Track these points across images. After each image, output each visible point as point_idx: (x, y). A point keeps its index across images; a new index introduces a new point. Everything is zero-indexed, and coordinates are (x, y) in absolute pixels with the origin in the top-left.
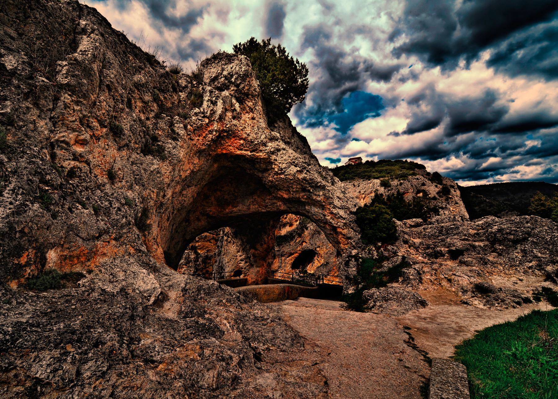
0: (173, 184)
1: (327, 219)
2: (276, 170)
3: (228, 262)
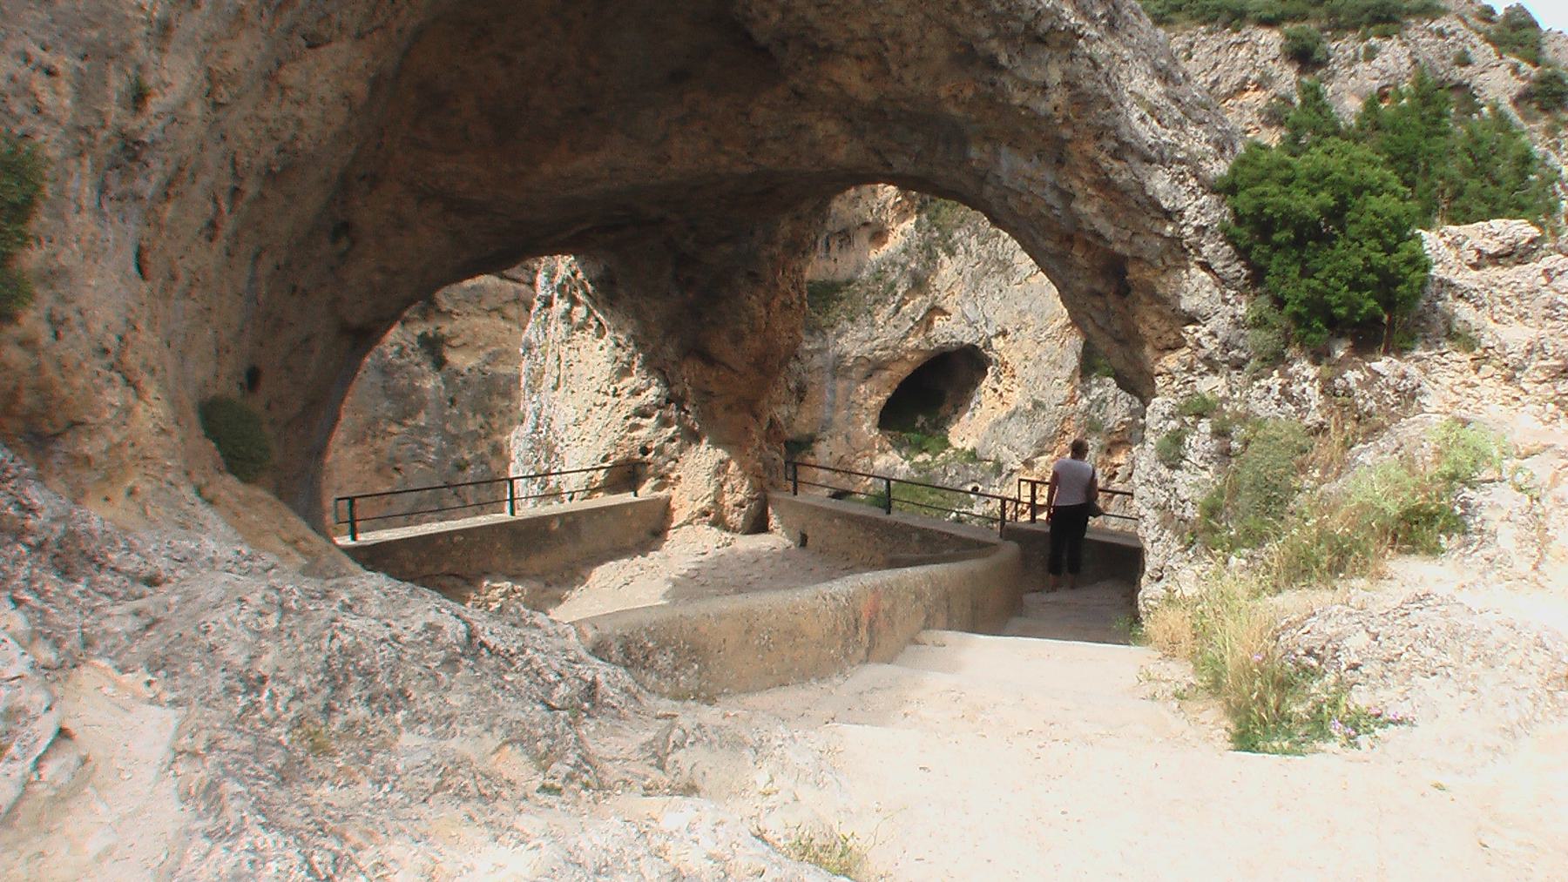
1: (1077, 219)
3: (577, 423)
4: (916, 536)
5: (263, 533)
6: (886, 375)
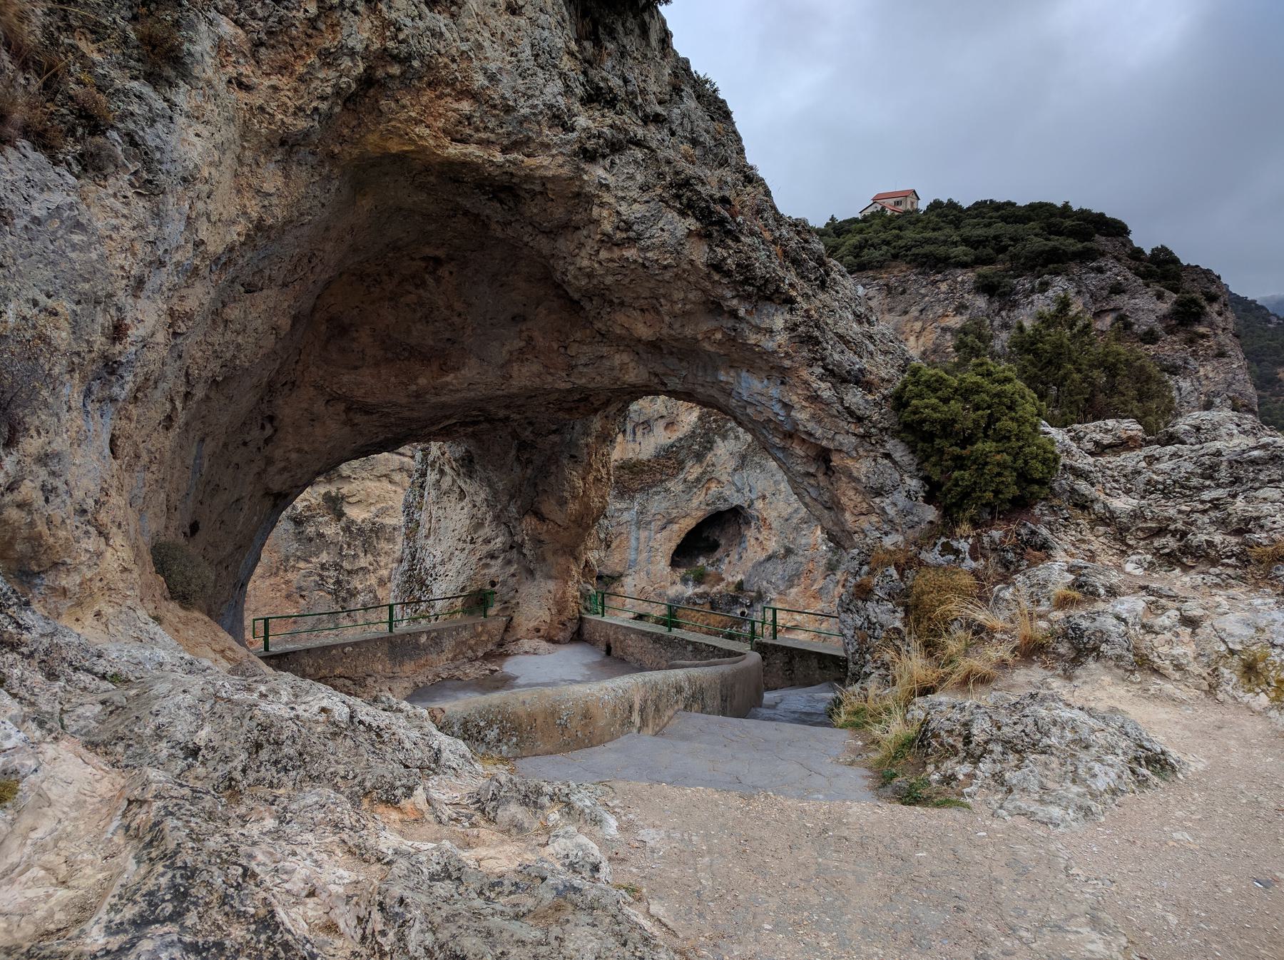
0: (163, 278)
1: (795, 423)
2: (607, 227)
3: (443, 563)
4: (690, 648)
5: (197, 645)
6: (676, 527)
